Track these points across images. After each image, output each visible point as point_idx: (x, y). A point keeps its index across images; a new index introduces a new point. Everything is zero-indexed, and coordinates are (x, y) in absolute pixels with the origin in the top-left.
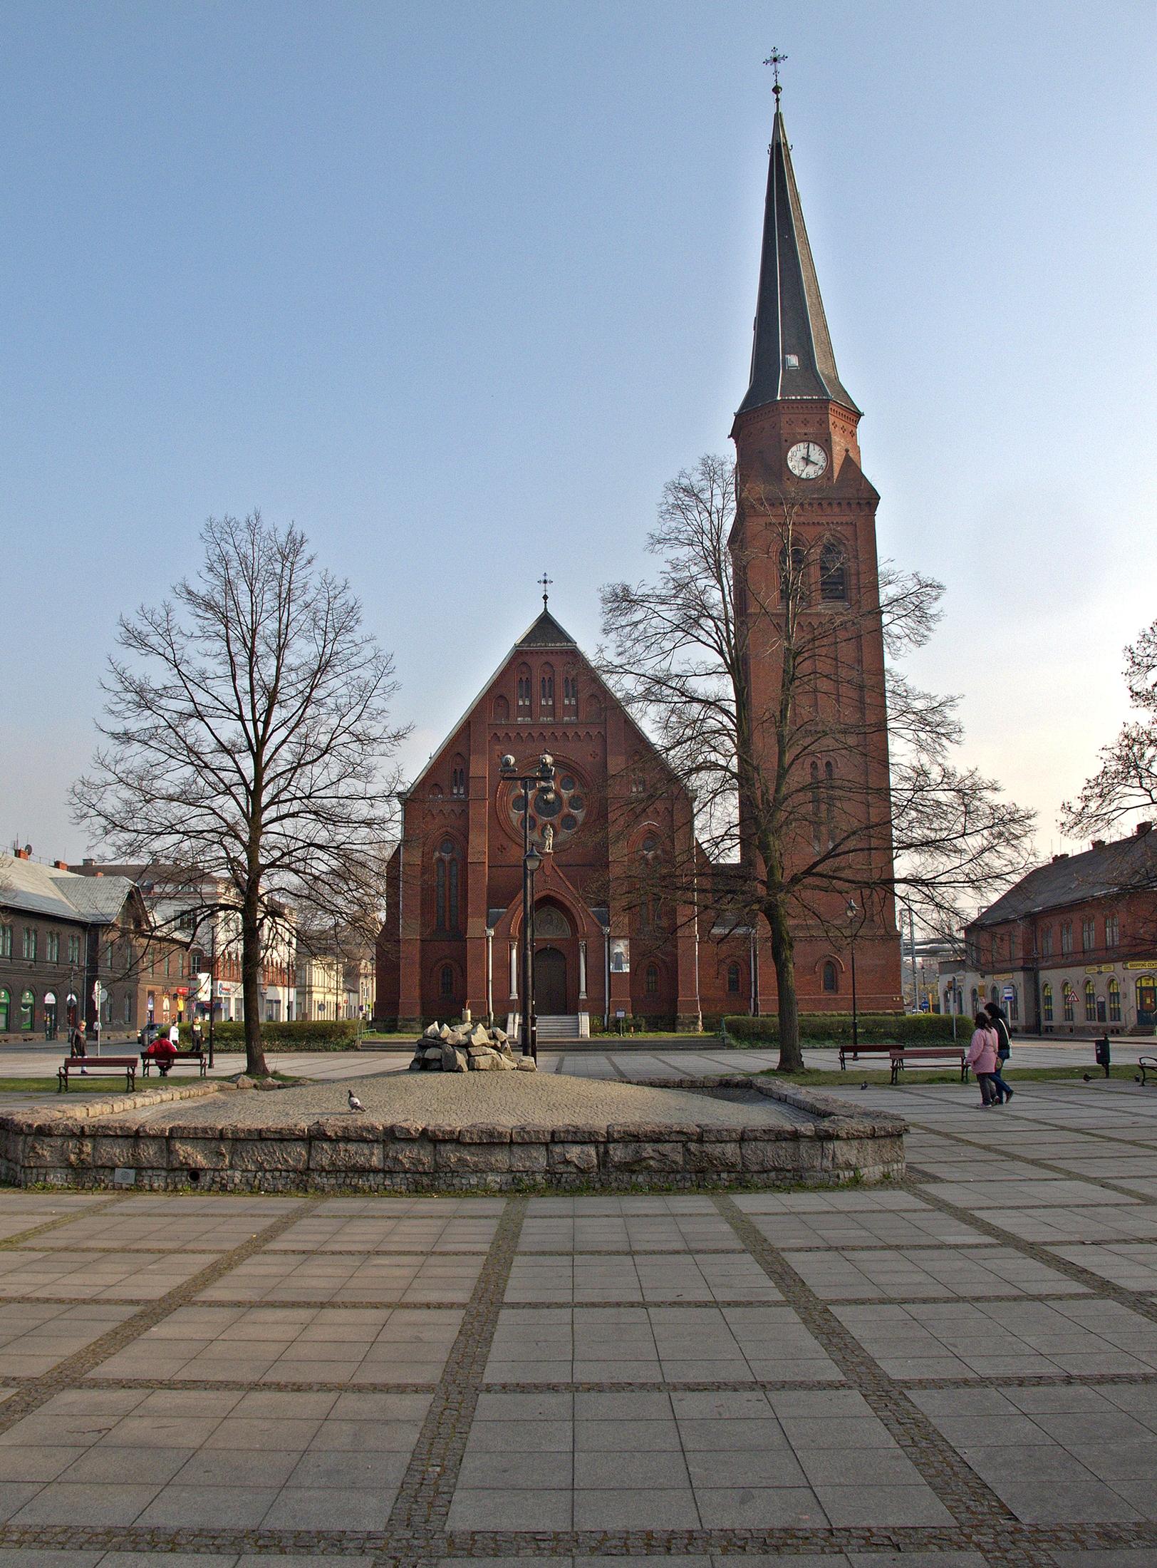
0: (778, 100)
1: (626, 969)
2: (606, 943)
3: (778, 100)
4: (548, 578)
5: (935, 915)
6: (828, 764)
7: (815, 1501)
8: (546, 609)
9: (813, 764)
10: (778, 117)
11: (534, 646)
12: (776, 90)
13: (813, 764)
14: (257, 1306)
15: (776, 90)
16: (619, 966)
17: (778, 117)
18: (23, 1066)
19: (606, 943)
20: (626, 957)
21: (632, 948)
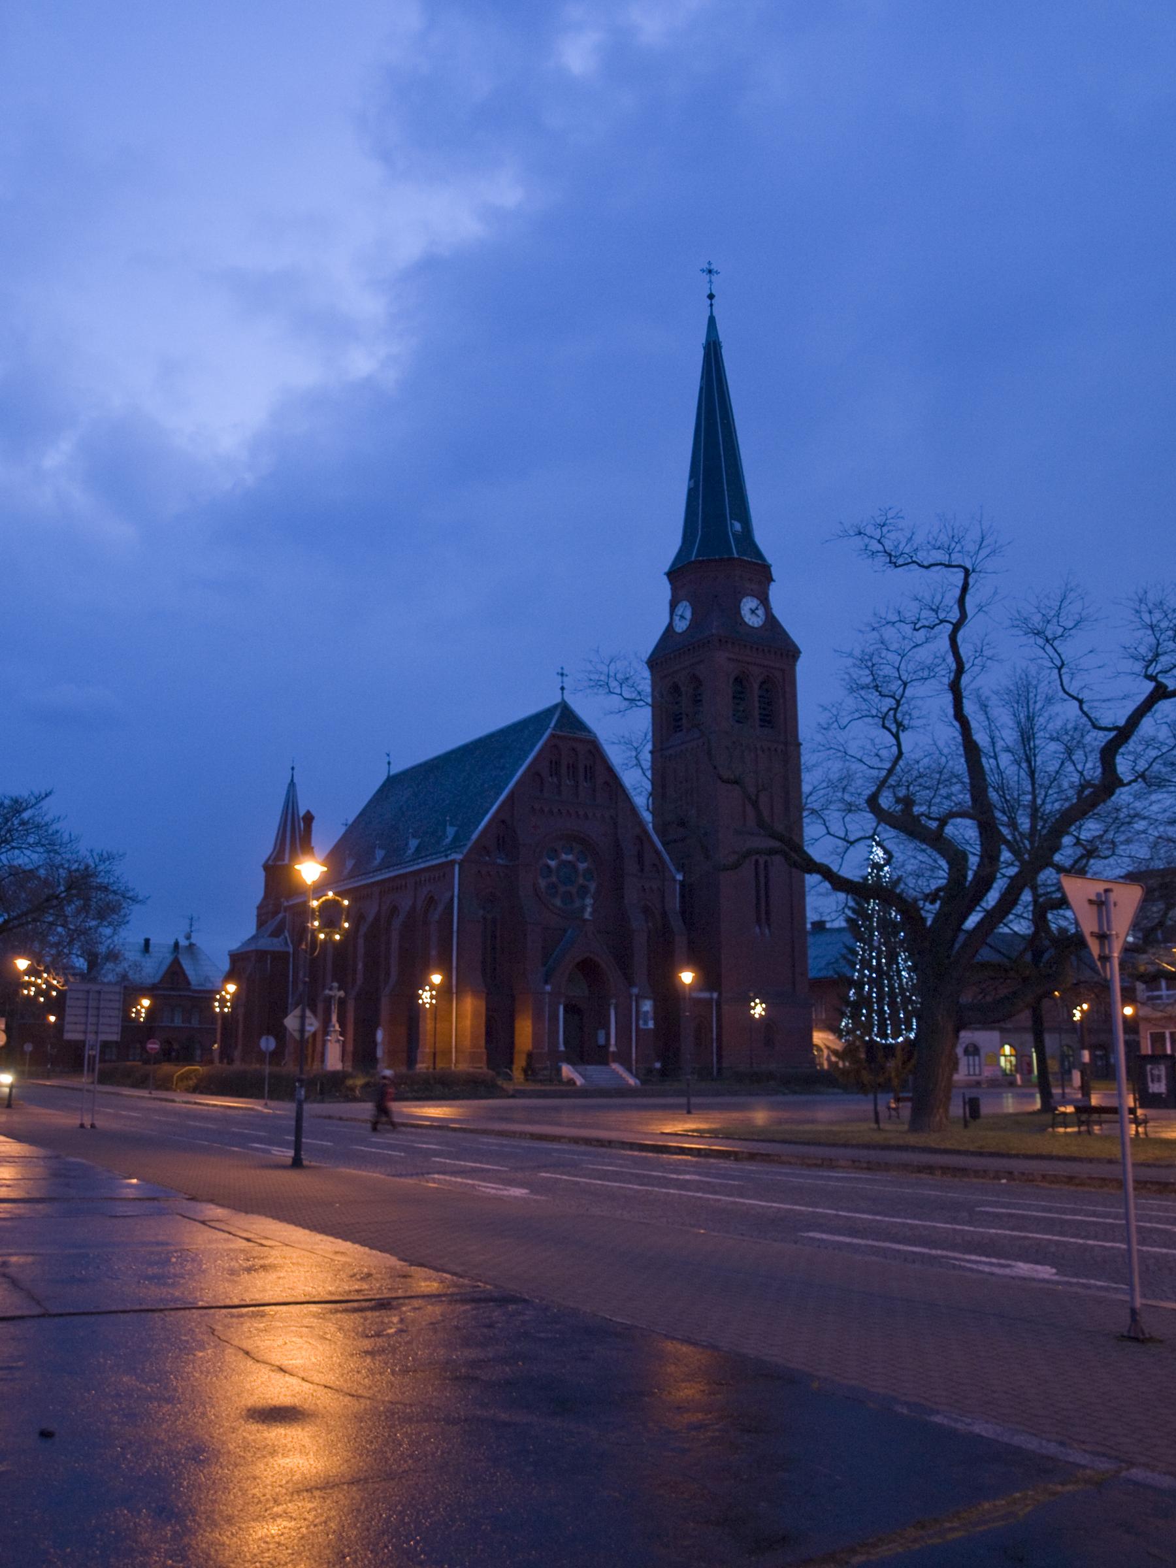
0: (711, 305)
1: (651, 1025)
2: (634, 1004)
3: (711, 305)
4: (565, 672)
5: (885, 671)
6: (766, 862)
7: (309, 1379)
8: (563, 699)
9: (757, 861)
10: (712, 321)
11: (634, 1071)
12: (711, 297)
13: (757, 861)
14: (949, 1168)
15: (711, 297)
16: (646, 1023)
17: (712, 321)
18: (967, 1257)
19: (634, 1004)
20: (651, 1015)
21: (655, 1007)
